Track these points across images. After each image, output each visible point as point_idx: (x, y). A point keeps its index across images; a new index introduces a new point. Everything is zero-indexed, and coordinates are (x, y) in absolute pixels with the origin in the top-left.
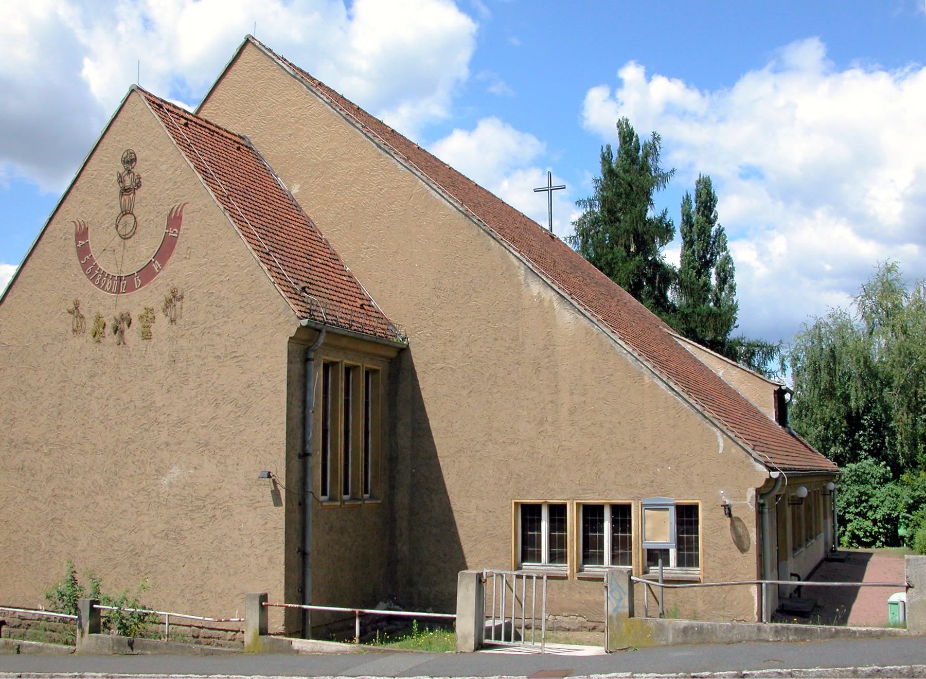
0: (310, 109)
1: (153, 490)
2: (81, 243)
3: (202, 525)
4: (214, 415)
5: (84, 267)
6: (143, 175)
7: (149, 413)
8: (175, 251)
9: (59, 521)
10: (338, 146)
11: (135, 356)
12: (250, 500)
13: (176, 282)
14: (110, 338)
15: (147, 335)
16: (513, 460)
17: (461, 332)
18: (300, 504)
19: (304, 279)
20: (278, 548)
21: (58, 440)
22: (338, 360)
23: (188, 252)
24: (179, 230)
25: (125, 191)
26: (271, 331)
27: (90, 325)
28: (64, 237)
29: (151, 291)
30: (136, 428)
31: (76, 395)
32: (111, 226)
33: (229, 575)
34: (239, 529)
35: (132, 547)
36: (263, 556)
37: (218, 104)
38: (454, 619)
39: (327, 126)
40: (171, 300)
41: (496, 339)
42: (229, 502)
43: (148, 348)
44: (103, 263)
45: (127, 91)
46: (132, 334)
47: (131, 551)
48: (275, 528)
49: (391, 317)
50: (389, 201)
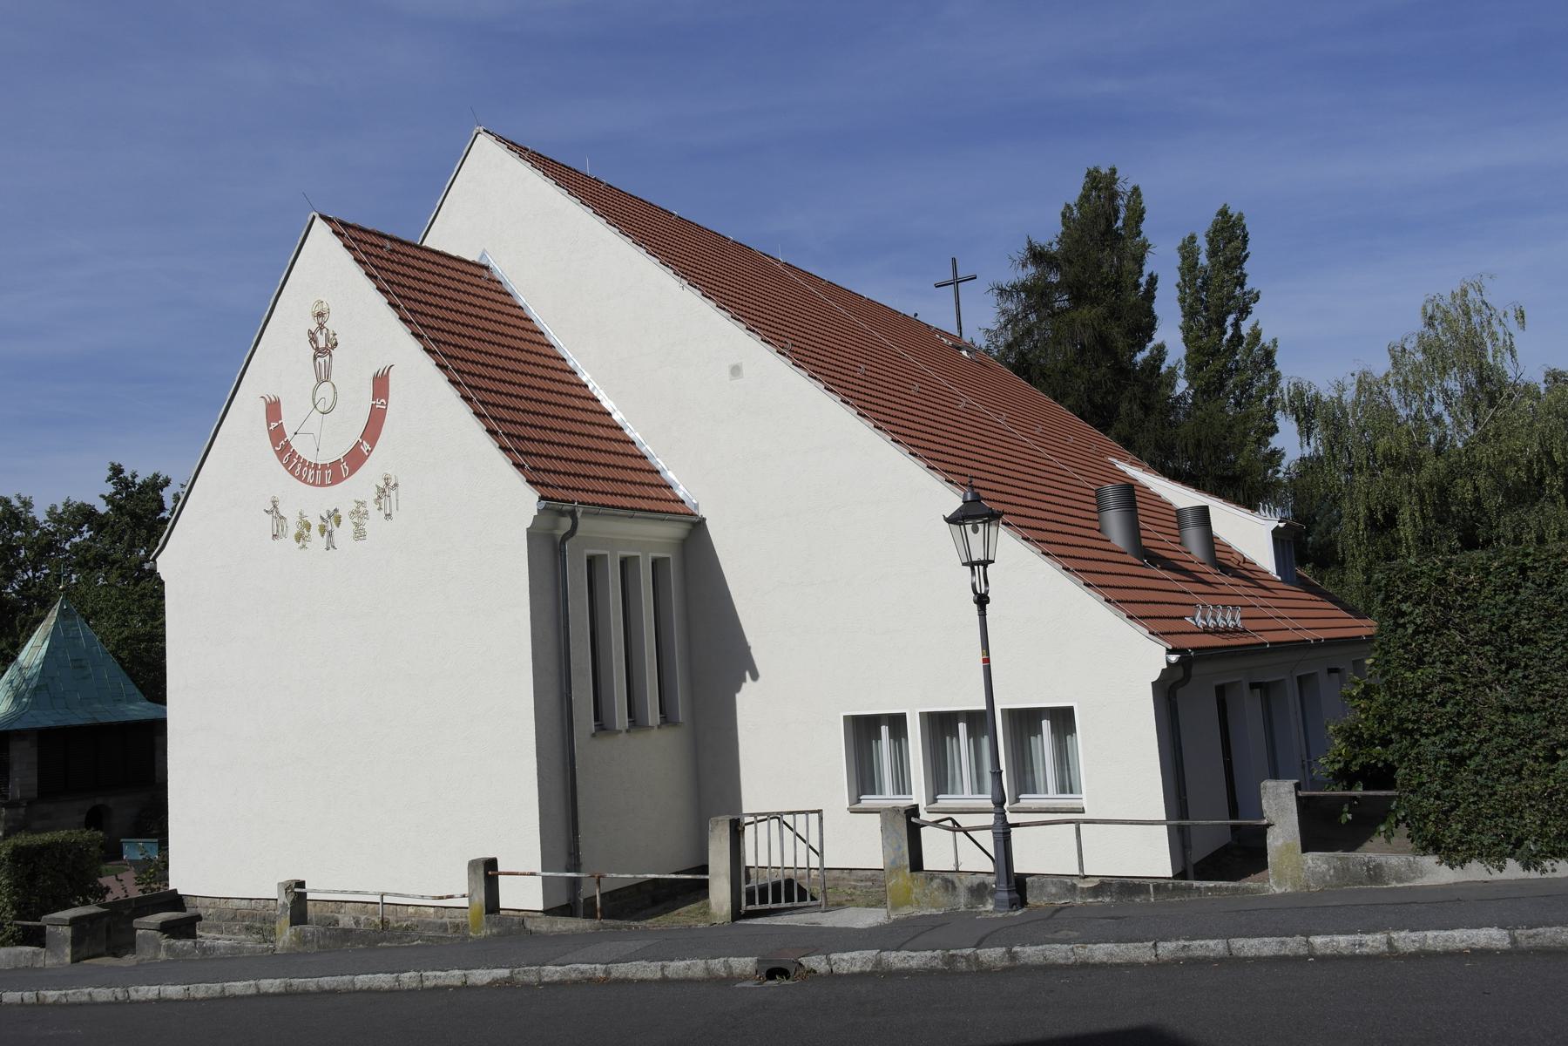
5: (280, 454)
14: (316, 540)
15: (360, 534)
25: (319, 352)
27: (293, 530)
38: (708, 880)
40: (384, 491)
44: (303, 448)
46: (343, 533)
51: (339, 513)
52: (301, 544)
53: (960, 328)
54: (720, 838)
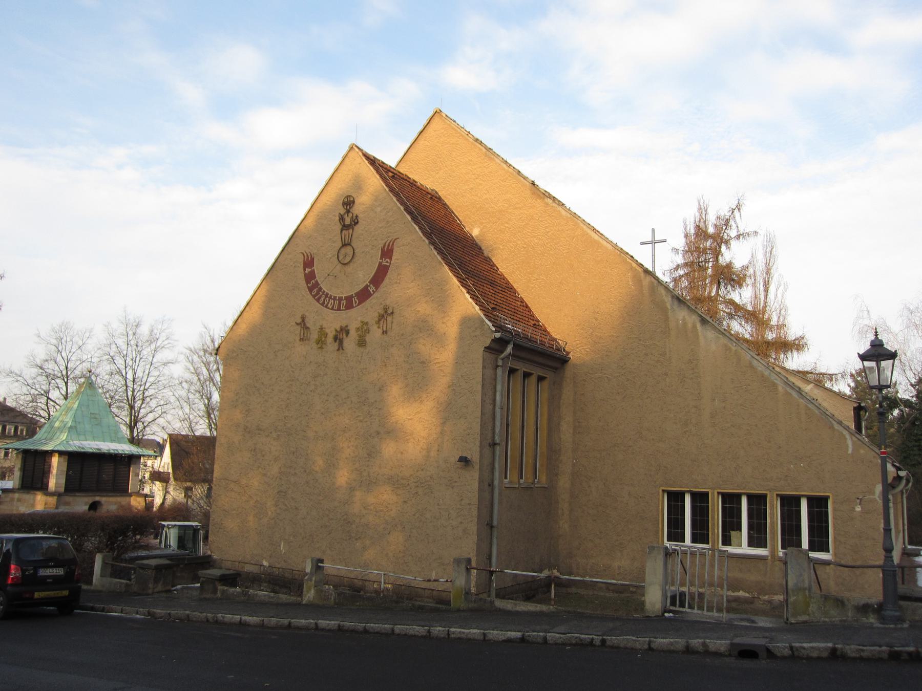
0: (488, 167)
1: (365, 470)
2: (308, 270)
3: (406, 500)
4: (419, 410)
6: (361, 216)
7: (363, 407)
8: (387, 277)
9: (284, 494)
10: (512, 197)
11: (352, 361)
12: (449, 480)
13: (388, 302)
14: (331, 346)
15: (362, 343)
16: (661, 454)
17: (616, 348)
18: (489, 485)
19: (492, 302)
20: (471, 521)
21: (285, 427)
22: (518, 368)
23: (399, 278)
24: (391, 260)
25: (345, 227)
26: (469, 342)
27: (314, 336)
28: (294, 265)
29: (367, 309)
30: (351, 419)
31: (302, 391)
32: (333, 256)
33: (428, 542)
34: (438, 505)
35: (345, 517)
36: (458, 527)
37: (412, 164)
39: (502, 181)
40: (383, 316)
41: (646, 355)
42: (430, 482)
43: (364, 354)
45: (347, 148)
46: (350, 343)
47: (344, 520)
48: (469, 504)
49: (556, 335)
50: (555, 242)
51: (348, 328)
52: (319, 346)
53: (654, 262)
54: (656, 560)
